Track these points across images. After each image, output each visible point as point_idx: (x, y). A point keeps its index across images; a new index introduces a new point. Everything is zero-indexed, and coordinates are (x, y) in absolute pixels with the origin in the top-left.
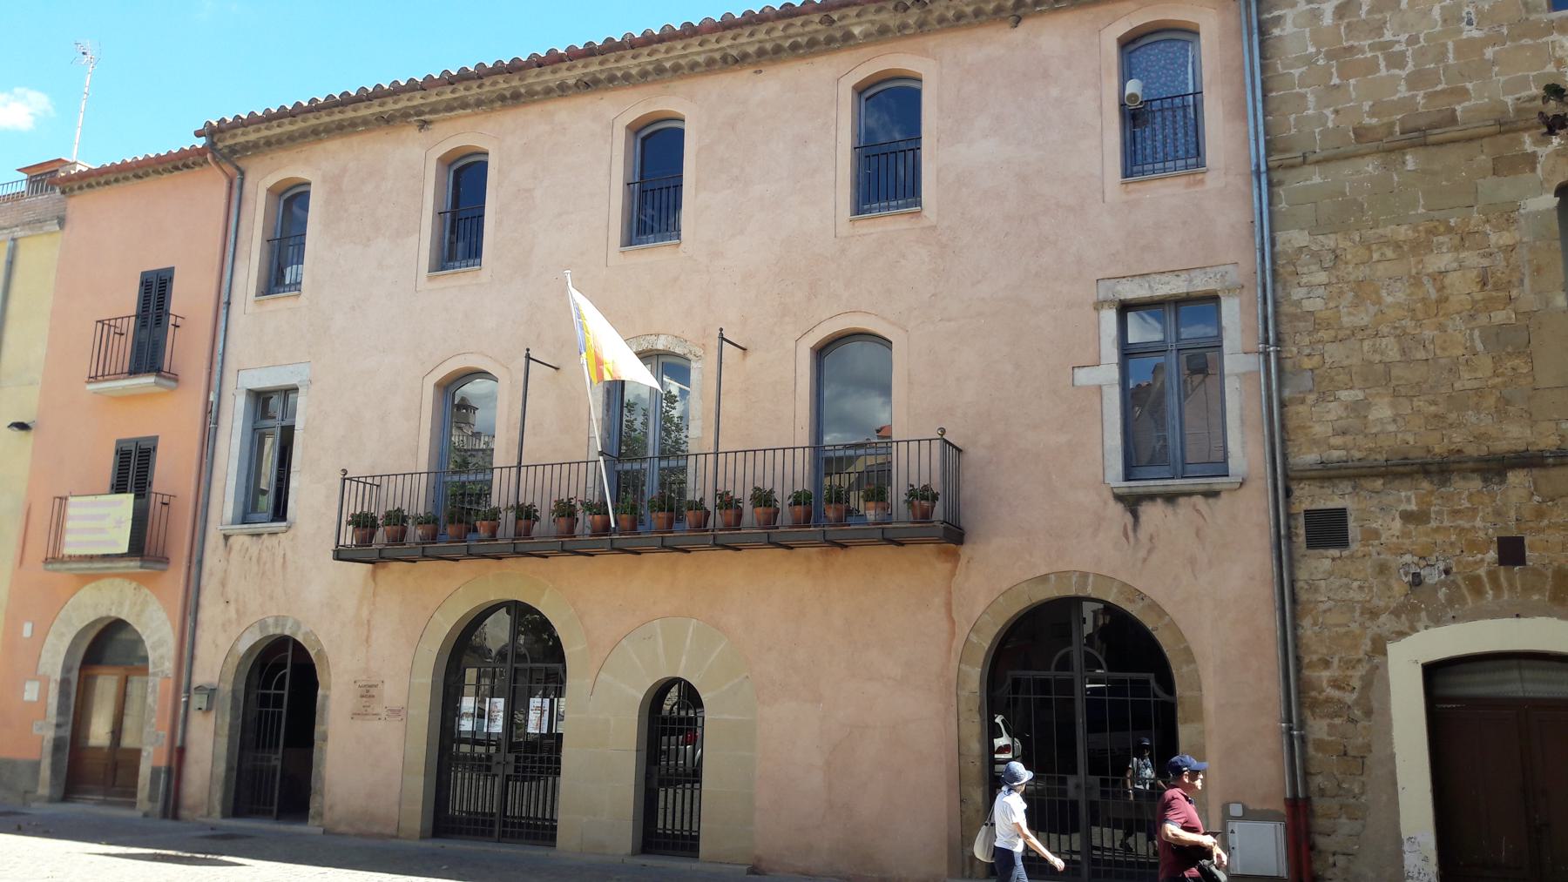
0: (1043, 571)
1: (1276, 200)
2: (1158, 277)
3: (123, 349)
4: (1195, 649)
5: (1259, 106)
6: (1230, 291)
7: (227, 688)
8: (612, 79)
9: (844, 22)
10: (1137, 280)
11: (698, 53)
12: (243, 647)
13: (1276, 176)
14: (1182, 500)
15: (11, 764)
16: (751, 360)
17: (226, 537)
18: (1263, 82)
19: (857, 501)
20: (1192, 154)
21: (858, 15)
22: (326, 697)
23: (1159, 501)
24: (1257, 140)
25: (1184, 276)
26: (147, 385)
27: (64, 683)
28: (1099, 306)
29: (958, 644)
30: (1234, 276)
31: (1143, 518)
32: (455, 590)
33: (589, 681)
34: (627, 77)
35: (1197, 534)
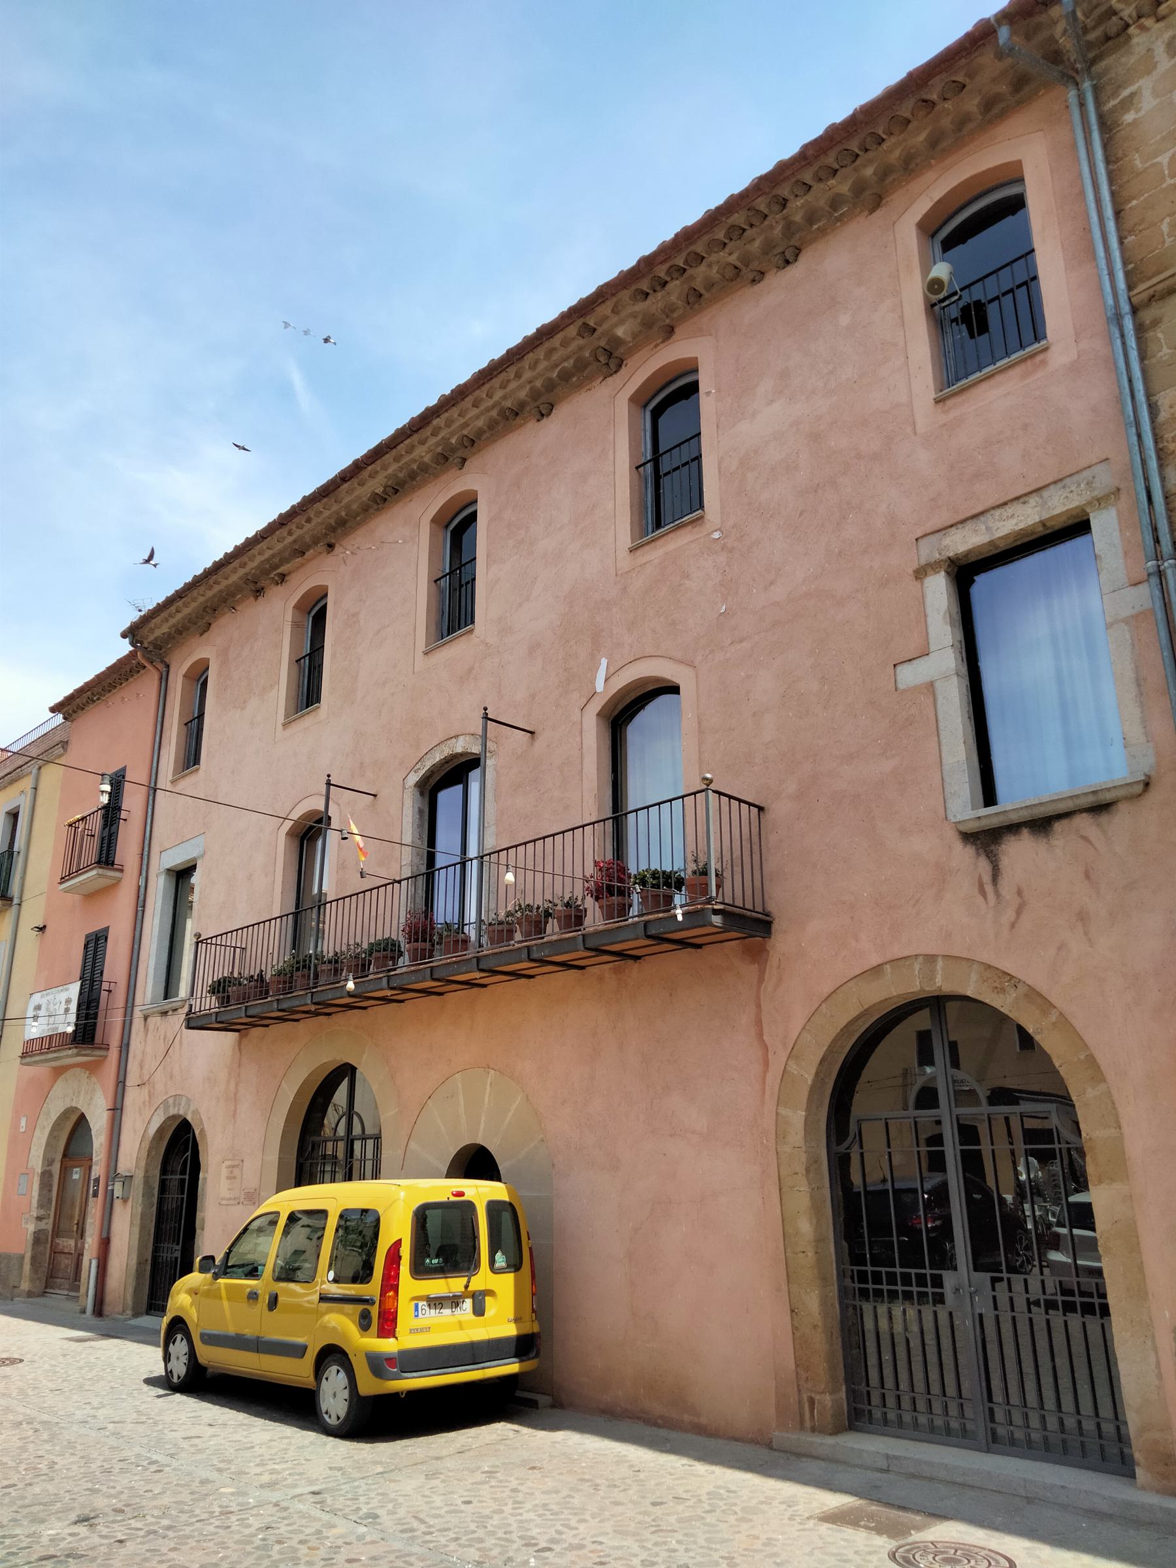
0: (875, 960)
1: (1152, 347)
2: (997, 512)
3: (91, 849)
4: (1103, 1060)
5: (1111, 225)
6: (1101, 501)
7: (140, 1175)
8: (412, 476)
9: (605, 326)
10: (970, 525)
11: (477, 417)
12: (152, 1130)
13: (1147, 316)
14: (1058, 826)
15: (8, 1257)
16: (541, 742)
17: (146, 1018)
18: (1113, 194)
19: (653, 924)
20: (1031, 328)
21: (615, 311)
22: (205, 1179)
23: (1025, 832)
24: (1111, 274)
25: (1033, 500)
26: (90, 880)
27: (46, 1175)
28: (921, 573)
29: (774, 1077)
30: (1105, 479)
31: (1005, 862)
32: (302, 1055)
33: (400, 1152)
34: (424, 468)
35: (1087, 876)
